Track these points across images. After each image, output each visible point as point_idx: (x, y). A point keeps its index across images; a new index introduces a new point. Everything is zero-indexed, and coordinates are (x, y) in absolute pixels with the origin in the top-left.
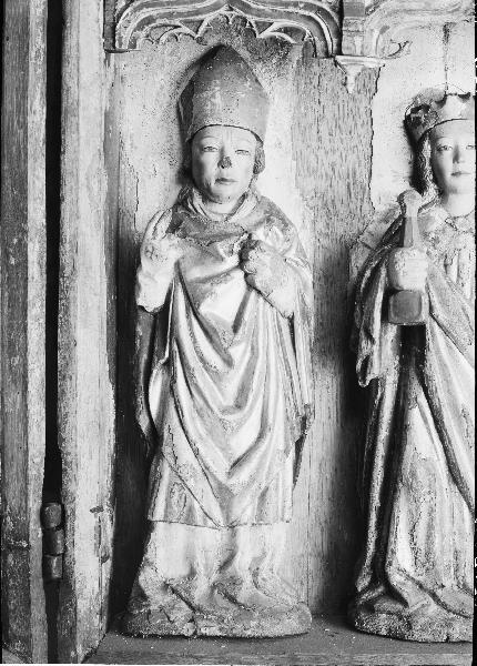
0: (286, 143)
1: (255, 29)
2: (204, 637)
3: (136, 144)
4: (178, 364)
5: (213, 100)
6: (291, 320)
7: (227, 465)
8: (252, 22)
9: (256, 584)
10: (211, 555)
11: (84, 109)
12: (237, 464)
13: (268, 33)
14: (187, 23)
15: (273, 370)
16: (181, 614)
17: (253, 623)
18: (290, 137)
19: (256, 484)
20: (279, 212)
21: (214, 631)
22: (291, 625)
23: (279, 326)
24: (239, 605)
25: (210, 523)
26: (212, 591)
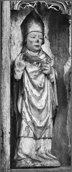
13: (51, 7)
14: (30, 4)
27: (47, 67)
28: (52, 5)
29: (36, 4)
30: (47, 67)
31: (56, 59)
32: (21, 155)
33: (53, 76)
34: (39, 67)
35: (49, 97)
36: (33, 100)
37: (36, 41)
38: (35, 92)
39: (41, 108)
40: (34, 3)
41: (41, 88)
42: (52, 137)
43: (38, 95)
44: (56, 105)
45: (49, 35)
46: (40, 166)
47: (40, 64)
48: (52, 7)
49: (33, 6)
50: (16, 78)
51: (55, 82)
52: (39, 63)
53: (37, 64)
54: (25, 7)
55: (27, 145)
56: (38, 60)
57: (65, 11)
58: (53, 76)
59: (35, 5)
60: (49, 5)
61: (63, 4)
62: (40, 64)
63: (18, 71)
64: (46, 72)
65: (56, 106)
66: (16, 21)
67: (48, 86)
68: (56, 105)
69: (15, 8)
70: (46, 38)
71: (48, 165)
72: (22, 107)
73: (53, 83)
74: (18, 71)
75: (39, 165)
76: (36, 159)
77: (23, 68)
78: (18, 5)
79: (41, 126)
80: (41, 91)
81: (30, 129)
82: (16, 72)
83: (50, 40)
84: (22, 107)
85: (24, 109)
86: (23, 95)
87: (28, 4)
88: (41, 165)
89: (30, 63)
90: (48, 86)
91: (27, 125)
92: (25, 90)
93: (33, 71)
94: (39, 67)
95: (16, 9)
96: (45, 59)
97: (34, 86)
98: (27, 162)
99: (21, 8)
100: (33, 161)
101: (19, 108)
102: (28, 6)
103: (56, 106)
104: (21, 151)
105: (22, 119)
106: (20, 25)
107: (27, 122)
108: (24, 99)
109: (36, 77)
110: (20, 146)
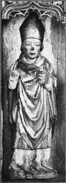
0: (50, 40)
1: (40, 13)
2: (28, 179)
3: (8, 40)
4: (10, 117)
5: (28, 68)
6: (50, 92)
7: (34, 133)
8: (39, 11)
9: (42, 165)
10: (30, 157)
11: (17, 80)
12: (37, 132)
13: (43, 14)
14: (21, 11)
15: (45, 106)
16: (22, 174)
17: (41, 175)
18: (50, 39)
19: (42, 138)
20: (48, 61)
21: (31, 177)
22: (51, 175)
23: (47, 94)
24: (37, 170)
25: (29, 149)
26: (31, 167)
27: (42, 77)
28: (46, 12)
29: (27, 12)
30: (42, 77)
31: (59, 63)
32: (15, 168)
33: (49, 86)
34: (35, 76)
35: (45, 106)
36: (27, 111)
37: (31, 48)
38: (29, 102)
39: (35, 120)
40: (26, 11)
41: (35, 100)
42: (26, 169)
43: (32, 106)
44: (54, 114)
45: (51, 37)
46: (32, 178)
47: (35, 73)
48: (45, 14)
49: (24, 14)
50: (10, 88)
51: (52, 91)
52: (34, 72)
53: (32, 73)
54: (15, 16)
55: (20, 157)
56: (34, 69)
57: (60, 18)
58: (49, 86)
59: (26, 12)
60: (42, 12)
61: (57, 10)
62: (35, 73)
63: (12, 81)
64: (41, 82)
65: (54, 116)
66: (14, 24)
67: (44, 95)
68: (54, 114)
69: (3, 18)
70: (47, 41)
71: (40, 178)
72: (17, 117)
73: (50, 92)
74: (12, 81)
75: (30, 177)
76: (29, 171)
77: (17, 78)
78: (7, 14)
79: (36, 137)
80: (36, 102)
81: (23, 140)
82: (10, 82)
83: (52, 44)
84: (17, 117)
85: (19, 121)
86: (18, 104)
87: (19, 11)
88: (33, 177)
89: (25, 72)
90: (44, 95)
91: (20, 137)
92: (19, 101)
93: (28, 80)
94: (35, 76)
95: (5, 18)
96: (42, 67)
97: (29, 97)
98: (19, 174)
99: (10, 17)
100: (26, 173)
101: (14, 117)
102: (18, 14)
103: (54, 116)
104: (14, 162)
105: (16, 131)
106: (18, 28)
107: (20, 134)
108: (18, 109)
109: (30, 88)
110: (13, 158)
